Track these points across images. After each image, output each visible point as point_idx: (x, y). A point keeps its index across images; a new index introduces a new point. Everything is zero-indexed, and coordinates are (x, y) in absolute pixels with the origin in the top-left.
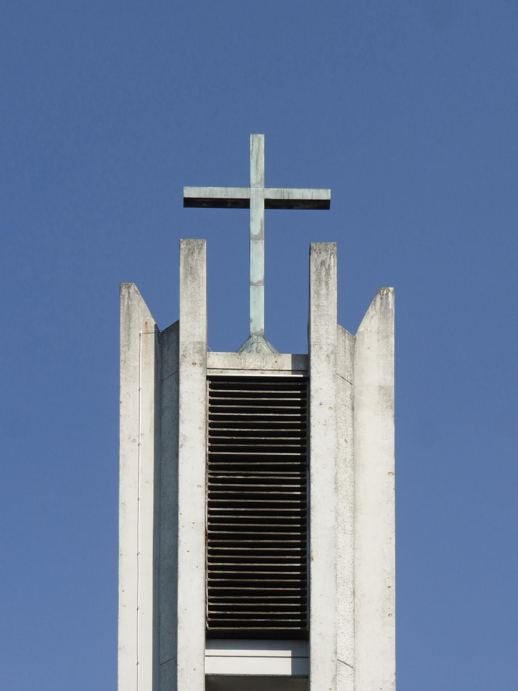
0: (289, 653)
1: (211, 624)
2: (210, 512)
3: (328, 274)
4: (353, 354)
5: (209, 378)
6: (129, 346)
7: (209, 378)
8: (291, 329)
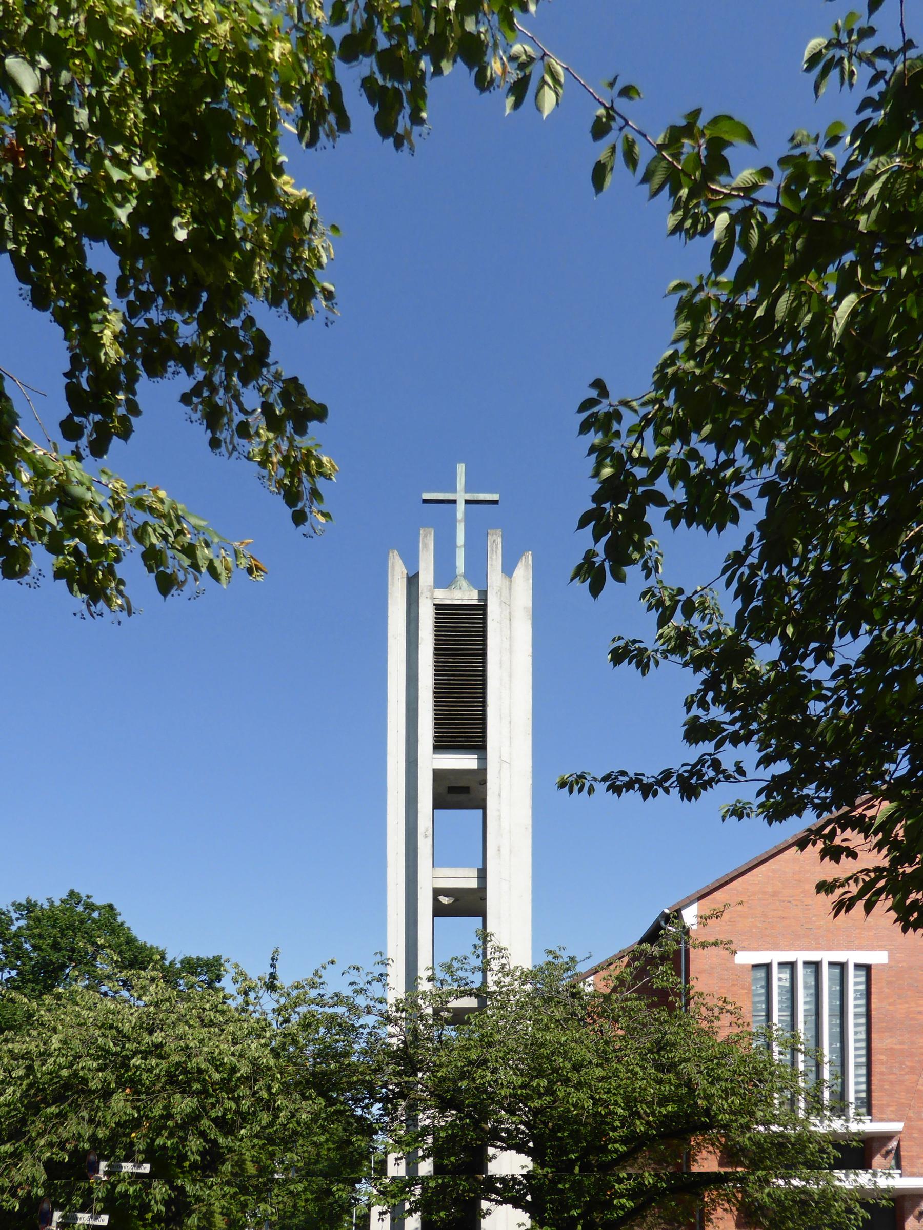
8: (477, 574)
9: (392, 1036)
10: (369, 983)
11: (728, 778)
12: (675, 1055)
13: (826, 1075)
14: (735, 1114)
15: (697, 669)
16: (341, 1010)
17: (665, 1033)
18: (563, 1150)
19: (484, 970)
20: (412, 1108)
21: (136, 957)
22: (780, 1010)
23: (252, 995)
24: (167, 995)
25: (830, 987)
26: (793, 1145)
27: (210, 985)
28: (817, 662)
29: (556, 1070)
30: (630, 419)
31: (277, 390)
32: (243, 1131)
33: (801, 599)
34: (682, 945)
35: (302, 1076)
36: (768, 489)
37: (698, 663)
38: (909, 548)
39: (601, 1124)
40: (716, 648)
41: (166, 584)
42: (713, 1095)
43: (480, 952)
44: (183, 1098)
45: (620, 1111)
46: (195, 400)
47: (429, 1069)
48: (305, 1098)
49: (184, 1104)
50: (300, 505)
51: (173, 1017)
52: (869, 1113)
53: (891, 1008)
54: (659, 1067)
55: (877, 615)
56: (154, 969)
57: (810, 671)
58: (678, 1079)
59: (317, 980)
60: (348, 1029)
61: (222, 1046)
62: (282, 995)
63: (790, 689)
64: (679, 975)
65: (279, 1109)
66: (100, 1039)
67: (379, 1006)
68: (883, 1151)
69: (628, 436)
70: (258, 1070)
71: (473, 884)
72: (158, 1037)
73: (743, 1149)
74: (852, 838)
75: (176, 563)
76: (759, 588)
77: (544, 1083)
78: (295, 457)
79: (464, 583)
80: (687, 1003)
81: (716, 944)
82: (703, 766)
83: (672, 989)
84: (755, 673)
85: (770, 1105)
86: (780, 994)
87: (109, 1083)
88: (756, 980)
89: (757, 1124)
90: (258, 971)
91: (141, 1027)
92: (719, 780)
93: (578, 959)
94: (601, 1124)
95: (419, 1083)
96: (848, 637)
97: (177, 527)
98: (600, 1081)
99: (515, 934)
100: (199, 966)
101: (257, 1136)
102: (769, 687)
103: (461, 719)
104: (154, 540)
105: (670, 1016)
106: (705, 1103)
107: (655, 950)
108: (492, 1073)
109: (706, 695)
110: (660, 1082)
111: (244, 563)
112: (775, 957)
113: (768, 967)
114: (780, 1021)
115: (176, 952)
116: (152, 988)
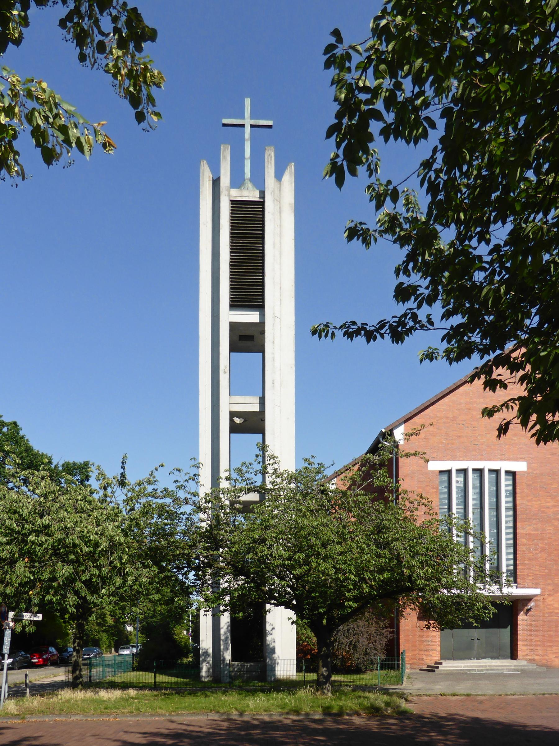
0: (258, 313)
1: (231, 301)
2: (231, 256)
3: (271, 160)
4: (280, 190)
5: (230, 200)
6: (203, 185)
7: (230, 200)
8: (259, 181)
9: (202, 521)
10: (186, 481)
11: (422, 327)
12: (389, 536)
13: (487, 552)
14: (428, 580)
15: (402, 246)
16: (168, 501)
17: (382, 520)
18: (315, 607)
19: (264, 473)
20: (215, 575)
21: (32, 461)
22: (457, 504)
23: (109, 490)
24: (52, 489)
25: (489, 488)
26: (466, 603)
27: (82, 482)
28: (479, 242)
29: (310, 547)
30: (356, 59)
31: (123, 18)
32: (103, 591)
33: (469, 195)
34: (394, 455)
35: (143, 551)
36: (446, 113)
37: (403, 241)
38: (538, 159)
39: (341, 585)
40: (414, 230)
41: (49, 156)
42: (414, 566)
43: (260, 459)
44: (63, 565)
45: (352, 577)
46: (69, 24)
47: (227, 546)
48: (145, 567)
49: (65, 570)
50: (141, 107)
51: (57, 505)
52: (515, 582)
53: (529, 504)
54: (379, 545)
55: (518, 208)
56: (44, 469)
57: (475, 249)
58: (391, 554)
59: (152, 479)
60: (173, 516)
61: (89, 527)
62: (129, 491)
63: (462, 262)
64: (392, 478)
65: (127, 574)
66: (7, 521)
67: (194, 499)
68: (525, 610)
69: (356, 71)
70: (113, 545)
71: (256, 408)
72: (46, 520)
73: (434, 607)
74: (501, 373)
75: (54, 139)
76: (441, 186)
77: (303, 556)
78: (137, 71)
79: (249, 185)
80: (397, 498)
81: (415, 454)
82: (406, 318)
83: (387, 487)
84: (440, 251)
85: (451, 573)
86: (457, 493)
87: (14, 554)
88: (441, 482)
89: (443, 588)
90: (112, 472)
91: (35, 513)
92: (416, 329)
93: (326, 466)
94: (341, 585)
95: (220, 556)
96: (499, 224)
97: (55, 111)
98: (340, 555)
99: (284, 446)
100: (75, 469)
101: (113, 594)
102: (451, 259)
103: (248, 289)
104: (40, 122)
105: (385, 507)
106: (408, 571)
107: (375, 459)
108: (269, 548)
109: (408, 265)
110: (379, 556)
111: (101, 139)
112: (454, 465)
113: (449, 472)
114: (457, 513)
115: (59, 459)
116: (43, 484)
